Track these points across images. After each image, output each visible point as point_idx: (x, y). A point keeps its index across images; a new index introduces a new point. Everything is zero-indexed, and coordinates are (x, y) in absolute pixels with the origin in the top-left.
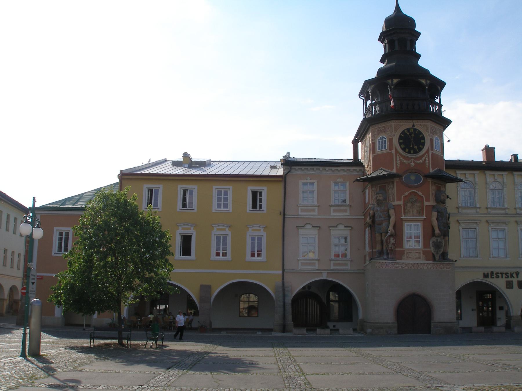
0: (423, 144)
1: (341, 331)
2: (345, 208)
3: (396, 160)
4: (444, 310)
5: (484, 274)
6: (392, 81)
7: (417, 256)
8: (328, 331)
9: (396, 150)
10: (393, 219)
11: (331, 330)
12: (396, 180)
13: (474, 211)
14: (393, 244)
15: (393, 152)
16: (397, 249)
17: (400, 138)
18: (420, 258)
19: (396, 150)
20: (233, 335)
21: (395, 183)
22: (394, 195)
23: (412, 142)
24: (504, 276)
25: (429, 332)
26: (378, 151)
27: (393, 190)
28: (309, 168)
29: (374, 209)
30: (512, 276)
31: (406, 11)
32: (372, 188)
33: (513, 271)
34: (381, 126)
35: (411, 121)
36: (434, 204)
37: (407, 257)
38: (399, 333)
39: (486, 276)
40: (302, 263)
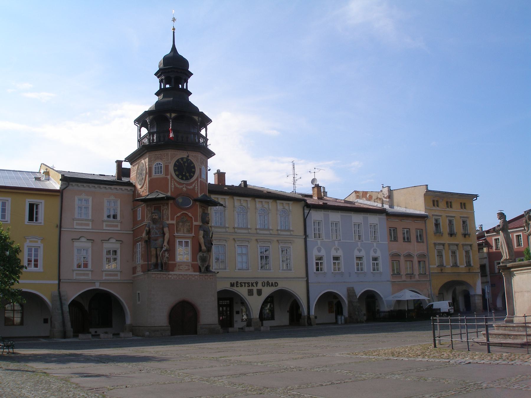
0: (194, 172)
1: (102, 336)
2: (116, 224)
3: (171, 185)
4: (209, 314)
5: (231, 283)
6: (171, 115)
7: (187, 268)
8: (90, 336)
9: (171, 176)
10: (167, 236)
11: (93, 336)
12: (171, 202)
13: (224, 230)
14: (167, 258)
15: (169, 177)
16: (170, 262)
17: (175, 165)
18: (189, 270)
19: (171, 176)
20: (23, 342)
21: (170, 205)
22: (168, 214)
23: (186, 170)
24: (246, 285)
25: (195, 333)
26: (154, 175)
27: (167, 210)
28: (85, 185)
29: (149, 226)
30: (252, 285)
31: (181, 52)
32: (147, 207)
33: (254, 281)
34: (158, 153)
35: (185, 152)
36: (201, 224)
37: (178, 269)
38: (172, 334)
39: (232, 285)
40: (76, 274)
